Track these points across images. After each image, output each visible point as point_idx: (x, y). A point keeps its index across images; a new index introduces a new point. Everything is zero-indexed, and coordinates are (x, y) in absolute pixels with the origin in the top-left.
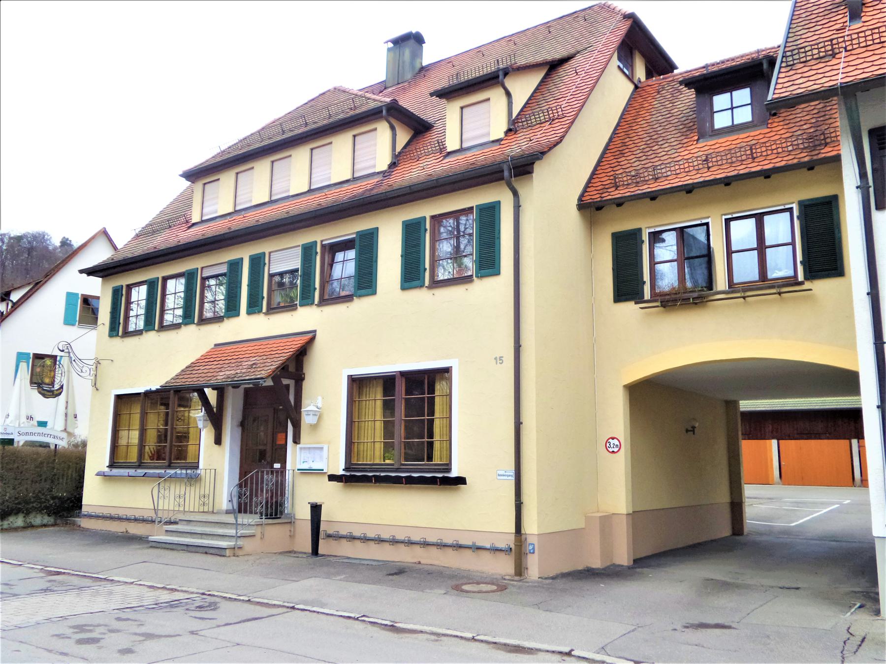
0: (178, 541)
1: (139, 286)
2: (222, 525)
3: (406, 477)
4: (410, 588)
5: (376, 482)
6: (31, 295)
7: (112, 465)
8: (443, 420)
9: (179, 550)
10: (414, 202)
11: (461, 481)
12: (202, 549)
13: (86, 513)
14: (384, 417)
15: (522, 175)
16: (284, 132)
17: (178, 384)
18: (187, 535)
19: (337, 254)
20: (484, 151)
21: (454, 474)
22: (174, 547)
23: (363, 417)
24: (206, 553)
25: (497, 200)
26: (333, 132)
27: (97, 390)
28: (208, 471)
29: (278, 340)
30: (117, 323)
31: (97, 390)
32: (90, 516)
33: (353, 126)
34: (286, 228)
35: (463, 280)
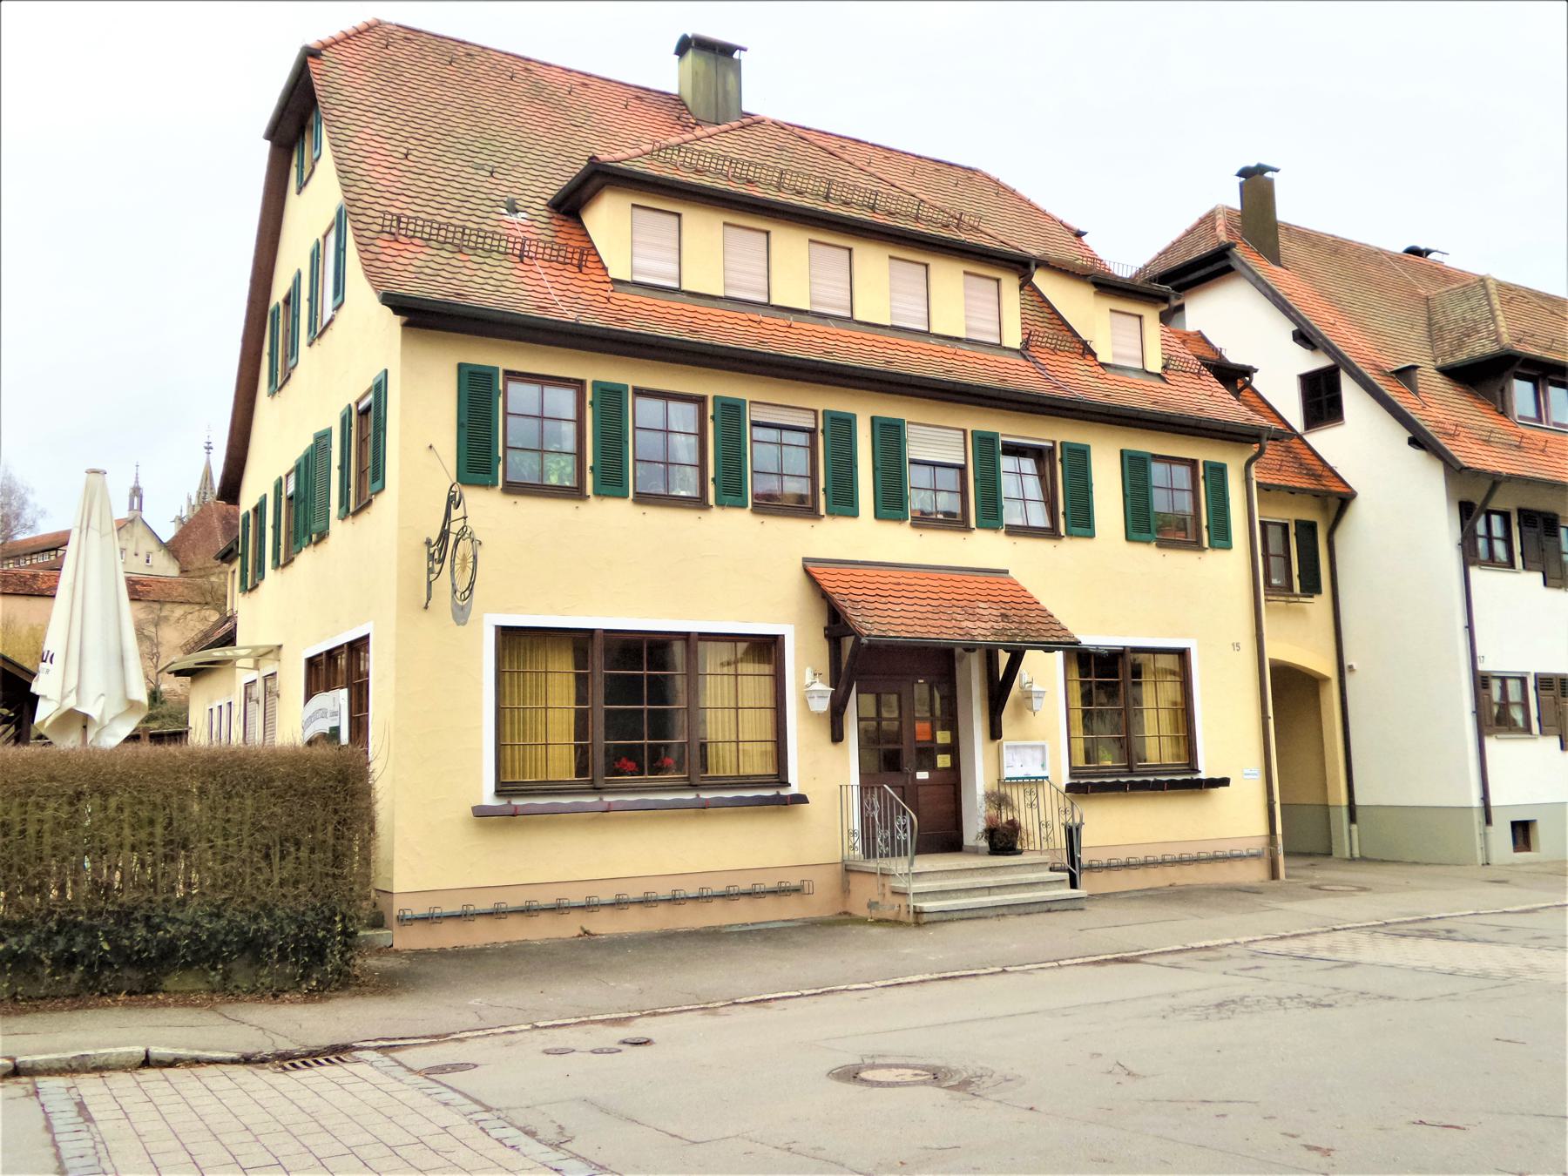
0: (992, 902)
1: (543, 385)
2: (1022, 868)
3: (1168, 782)
4: (348, 1002)
5: (1131, 789)
6: (1236, 441)
7: (502, 789)
8: (722, 713)
9: (991, 917)
10: (746, 375)
11: (801, 799)
12: (1038, 906)
13: (1238, 852)
14: (1083, 705)
15: (618, 354)
16: (827, 198)
17: (909, 635)
18: (1022, 888)
19: (1032, 460)
20: (989, 357)
21: (794, 789)
22: (981, 913)
23: (507, 702)
24: (1049, 911)
25: (1222, 462)
26: (707, 203)
27: (426, 607)
28: (849, 788)
29: (982, 578)
30: (1211, 528)
31: (426, 607)
32: (404, 920)
33: (1131, 298)
34: (1060, 411)
35: (575, 493)
